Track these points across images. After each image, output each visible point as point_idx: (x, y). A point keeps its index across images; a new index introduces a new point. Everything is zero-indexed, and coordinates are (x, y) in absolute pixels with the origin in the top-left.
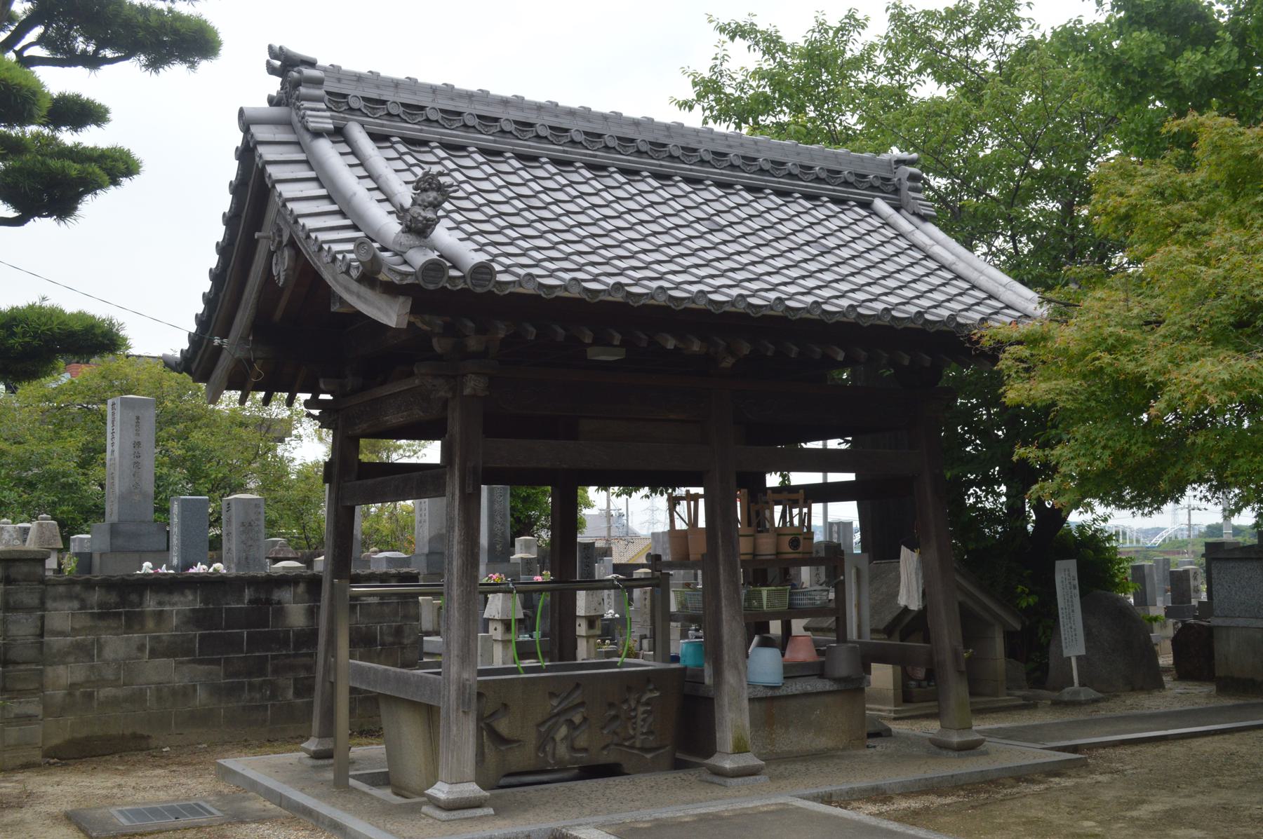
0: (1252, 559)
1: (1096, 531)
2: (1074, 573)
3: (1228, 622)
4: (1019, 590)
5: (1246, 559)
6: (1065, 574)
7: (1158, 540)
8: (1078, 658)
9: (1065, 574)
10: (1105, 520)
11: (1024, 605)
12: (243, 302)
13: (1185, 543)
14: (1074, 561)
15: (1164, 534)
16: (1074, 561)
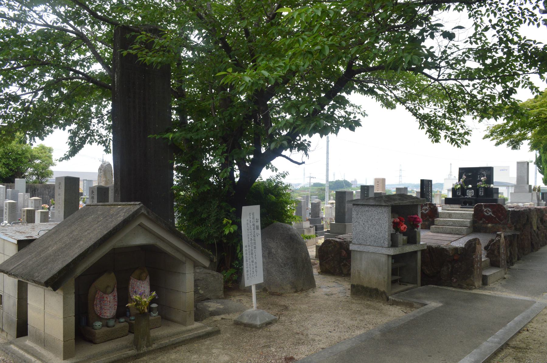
0: (381, 206)
1: (278, 183)
2: (258, 216)
3: (361, 248)
4: (225, 222)
5: (378, 205)
6: (251, 215)
7: (299, 187)
8: (258, 286)
9: (251, 215)
10: (284, 176)
11: (227, 232)
12: (440, 234)
13: (308, 188)
14: (258, 207)
15: (301, 186)
16: (258, 207)
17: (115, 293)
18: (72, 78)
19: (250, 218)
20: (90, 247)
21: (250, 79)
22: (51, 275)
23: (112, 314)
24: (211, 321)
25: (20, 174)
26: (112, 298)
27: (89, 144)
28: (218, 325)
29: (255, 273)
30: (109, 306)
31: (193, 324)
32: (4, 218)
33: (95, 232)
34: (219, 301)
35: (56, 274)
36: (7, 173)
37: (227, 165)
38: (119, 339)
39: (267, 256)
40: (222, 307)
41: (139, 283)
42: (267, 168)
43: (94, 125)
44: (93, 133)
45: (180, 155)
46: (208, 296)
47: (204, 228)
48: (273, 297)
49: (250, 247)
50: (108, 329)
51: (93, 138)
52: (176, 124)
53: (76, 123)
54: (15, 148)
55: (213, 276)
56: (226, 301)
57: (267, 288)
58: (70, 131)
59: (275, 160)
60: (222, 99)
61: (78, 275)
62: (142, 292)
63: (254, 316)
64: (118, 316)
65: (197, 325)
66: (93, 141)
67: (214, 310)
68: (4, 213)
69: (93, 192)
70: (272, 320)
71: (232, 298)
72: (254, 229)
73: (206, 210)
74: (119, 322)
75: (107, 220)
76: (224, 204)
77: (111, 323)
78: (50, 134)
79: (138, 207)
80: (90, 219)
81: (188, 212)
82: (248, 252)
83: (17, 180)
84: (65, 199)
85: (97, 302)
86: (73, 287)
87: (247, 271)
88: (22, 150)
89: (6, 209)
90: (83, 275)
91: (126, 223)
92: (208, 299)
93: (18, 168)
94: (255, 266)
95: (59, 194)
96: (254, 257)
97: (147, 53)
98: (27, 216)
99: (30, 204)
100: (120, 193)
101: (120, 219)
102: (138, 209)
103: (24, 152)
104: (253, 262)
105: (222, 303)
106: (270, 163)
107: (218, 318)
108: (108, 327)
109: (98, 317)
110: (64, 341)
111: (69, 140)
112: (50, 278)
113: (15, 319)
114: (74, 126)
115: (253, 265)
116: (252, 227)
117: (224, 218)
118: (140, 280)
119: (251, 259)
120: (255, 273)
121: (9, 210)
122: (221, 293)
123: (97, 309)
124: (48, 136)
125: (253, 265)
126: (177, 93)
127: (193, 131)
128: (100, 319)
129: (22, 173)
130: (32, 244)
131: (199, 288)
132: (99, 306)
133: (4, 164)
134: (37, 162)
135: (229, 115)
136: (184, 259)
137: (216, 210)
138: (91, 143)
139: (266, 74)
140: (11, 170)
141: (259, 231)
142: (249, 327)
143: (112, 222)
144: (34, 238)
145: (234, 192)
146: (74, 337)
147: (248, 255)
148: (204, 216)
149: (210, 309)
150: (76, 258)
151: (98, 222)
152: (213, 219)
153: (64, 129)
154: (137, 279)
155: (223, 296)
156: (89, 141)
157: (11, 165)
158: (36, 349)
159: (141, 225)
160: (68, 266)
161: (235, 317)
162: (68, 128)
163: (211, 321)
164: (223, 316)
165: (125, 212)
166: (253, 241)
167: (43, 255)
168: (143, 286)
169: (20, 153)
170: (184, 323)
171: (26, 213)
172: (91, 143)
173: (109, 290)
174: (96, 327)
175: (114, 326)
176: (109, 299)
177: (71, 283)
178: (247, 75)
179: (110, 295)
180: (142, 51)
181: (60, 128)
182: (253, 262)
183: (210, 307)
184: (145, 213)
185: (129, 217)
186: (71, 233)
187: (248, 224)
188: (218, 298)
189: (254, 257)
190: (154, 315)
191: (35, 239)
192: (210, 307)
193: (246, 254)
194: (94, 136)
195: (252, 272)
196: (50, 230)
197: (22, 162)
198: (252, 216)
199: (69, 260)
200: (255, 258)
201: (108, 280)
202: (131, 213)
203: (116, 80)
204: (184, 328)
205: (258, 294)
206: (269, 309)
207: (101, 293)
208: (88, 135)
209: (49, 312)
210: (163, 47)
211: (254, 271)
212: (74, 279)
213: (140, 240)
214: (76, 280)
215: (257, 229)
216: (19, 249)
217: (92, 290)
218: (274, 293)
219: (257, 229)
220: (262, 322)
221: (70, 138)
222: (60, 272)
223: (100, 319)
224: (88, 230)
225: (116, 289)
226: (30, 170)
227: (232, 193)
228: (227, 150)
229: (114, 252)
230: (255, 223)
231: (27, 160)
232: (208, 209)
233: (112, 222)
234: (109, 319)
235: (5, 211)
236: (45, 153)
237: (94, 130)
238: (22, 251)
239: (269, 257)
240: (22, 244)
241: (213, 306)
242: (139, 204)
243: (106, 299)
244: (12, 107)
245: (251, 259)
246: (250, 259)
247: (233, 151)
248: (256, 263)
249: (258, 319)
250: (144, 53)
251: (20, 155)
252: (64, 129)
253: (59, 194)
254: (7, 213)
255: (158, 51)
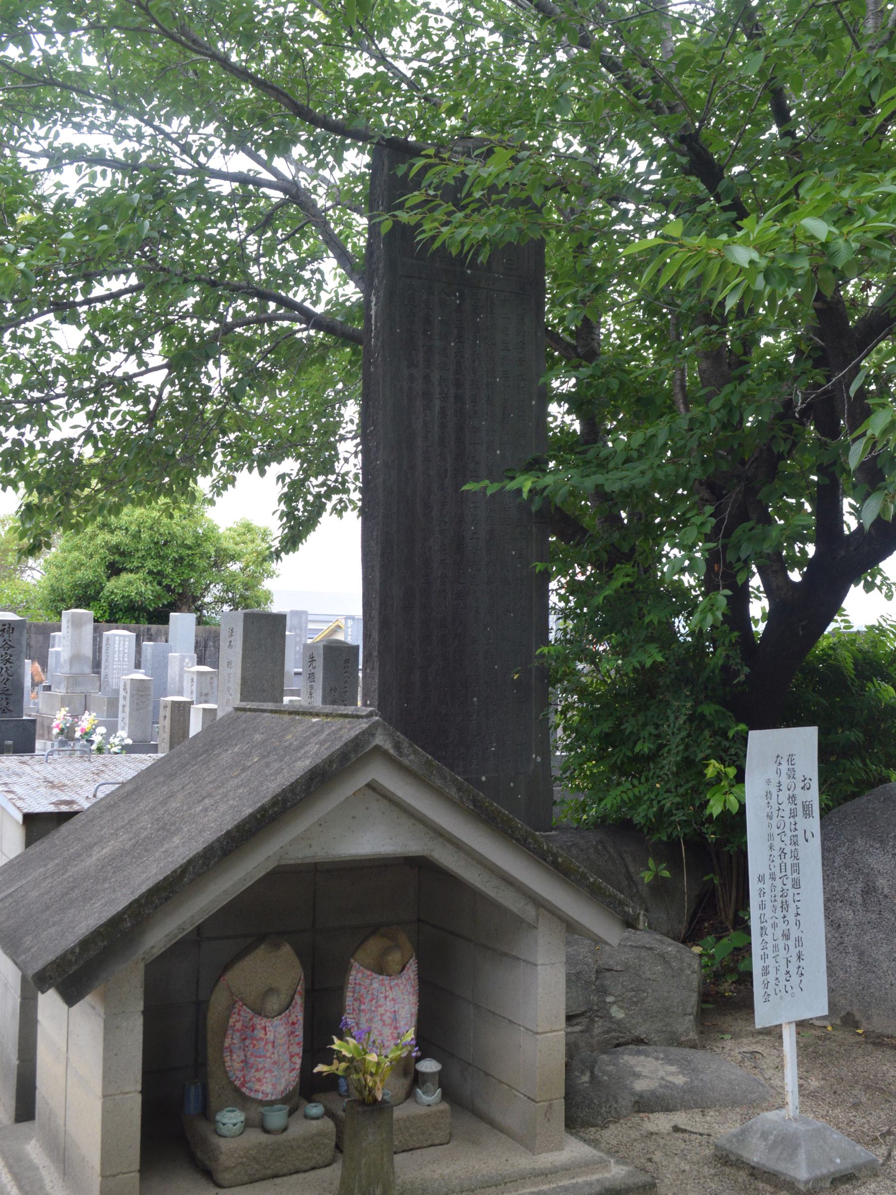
2: (808, 764)
4: (710, 772)
17: (298, 1013)
18: (271, 320)
19: (779, 772)
20: (190, 862)
21: (755, 256)
22: (59, 951)
23: (281, 1088)
24: (634, 1134)
25: (185, 599)
26: (282, 1030)
27: (334, 516)
28: (658, 1156)
29: (795, 979)
30: (268, 1056)
31: (560, 1147)
32: (120, 724)
33: (223, 808)
34: (676, 1052)
35: (72, 951)
36: (158, 597)
37: (723, 575)
38: (300, 1176)
39: (859, 900)
40: (680, 1080)
41: (377, 983)
42: (869, 587)
43: (346, 460)
44: (344, 482)
45: (577, 545)
46: (641, 1031)
47: (643, 788)
48: (879, 1054)
49: (778, 883)
50: (264, 1138)
51: (345, 497)
52: (567, 444)
53: (298, 456)
54: (177, 530)
55: (663, 958)
56: (698, 1056)
57: (858, 1016)
58: (281, 477)
59: (889, 559)
60: (706, 356)
61: (157, 952)
62: (384, 1013)
63: (786, 1143)
64: (310, 1087)
65: (575, 1150)
66: (345, 508)
67: (653, 1092)
68: (120, 708)
69: (312, 659)
70: (859, 1168)
71: (729, 1044)
72: (793, 814)
73: (651, 729)
74: (306, 1117)
75: (267, 765)
76: (708, 709)
77: (276, 1118)
78: (230, 486)
79: (364, 725)
80: (226, 757)
81: (596, 731)
82: (767, 898)
83: (172, 615)
84: (244, 679)
85: (232, 1040)
86: (139, 992)
87: (765, 971)
88: (197, 537)
89: (125, 698)
90: (181, 948)
91: (319, 780)
92: (639, 1041)
93: (184, 583)
94: (794, 952)
95: (229, 663)
96: (791, 916)
97: (450, 214)
98: (172, 720)
99: (186, 684)
100: (377, 665)
101: (303, 765)
102: (363, 733)
103: (199, 541)
104: (786, 936)
105: (686, 1066)
106: (880, 572)
107: (661, 1122)
108: (266, 1131)
109: (237, 1090)
110: (104, 1176)
111: (283, 507)
112: (223, 908)
113: (15, 1062)
114: (291, 466)
115: (787, 948)
116: (787, 807)
117: (707, 758)
118: (381, 973)
119: (782, 926)
120: (795, 979)
121: (132, 702)
122: (686, 1026)
123: (234, 1063)
124: (224, 493)
125: (787, 948)
126: (574, 348)
127: (611, 465)
128: (241, 1099)
129: (195, 599)
130: (65, 828)
131: (610, 999)
132: (238, 1056)
133: (150, 572)
134: (234, 567)
135: (724, 406)
136: (530, 912)
137: (684, 733)
138: (340, 513)
139: (820, 228)
140: (168, 588)
141: (814, 824)
142: (768, 1182)
143: (279, 771)
144: (75, 808)
145: (747, 670)
146: (136, 1166)
147: (768, 912)
148: (644, 747)
149: (640, 1086)
150: (141, 897)
151: (244, 770)
152: (670, 762)
153: (262, 473)
154: (372, 970)
155: (693, 1035)
156: (334, 508)
157: (167, 576)
158: (41, 1180)
159: (372, 786)
160: (115, 922)
161: (723, 1127)
162: (274, 469)
163: (634, 1134)
164: (680, 1118)
165: (322, 743)
166: (789, 861)
167: (72, 871)
168: (391, 995)
169: (188, 542)
170: (526, 1141)
171: (169, 709)
172: (340, 513)
173: (273, 1003)
174: (224, 1130)
175: (285, 1129)
176: (270, 1036)
177: (129, 978)
178: (745, 242)
179: (276, 1021)
180: (432, 210)
181: (250, 469)
182: (786, 936)
183: (637, 1076)
184: (388, 746)
185: (329, 761)
186: (164, 803)
187: (768, 794)
188: (674, 1041)
189: (791, 916)
190: (426, 1099)
191: (76, 813)
192: (637, 1076)
193: (762, 906)
194: (347, 491)
195: (782, 977)
196: (123, 784)
197: (192, 567)
198: (784, 767)
199: (122, 900)
200: (798, 923)
201: (275, 970)
202: (338, 745)
203: (373, 313)
204: (523, 1162)
205: (803, 1049)
206: (856, 1106)
207: (246, 1013)
208: (331, 491)
209: (83, 1058)
210: (492, 189)
211: (793, 969)
212: (142, 966)
213: (373, 839)
214: (148, 967)
215: (807, 813)
216: (30, 840)
217: (219, 1000)
218: (880, 1036)
219: (807, 813)
220: (818, 1173)
221: (287, 498)
222: (85, 944)
223: (241, 1099)
224: (209, 795)
225: (299, 1000)
226: (216, 590)
227: (737, 674)
228: (716, 528)
229: (279, 876)
230: (798, 792)
231: (203, 564)
232: (657, 726)
233: (279, 771)
234: (271, 1103)
235: (121, 702)
236: (253, 541)
237: (347, 473)
238: (38, 847)
239: (864, 904)
240: (37, 825)
241: (650, 1071)
242: (370, 715)
243: (261, 1034)
244: (117, 413)
245: (782, 926)
246: (774, 926)
247: (738, 532)
248: (799, 940)
249: (802, 1156)
250: (440, 214)
251: (190, 548)
252: (262, 473)
253: (229, 663)
254: (127, 709)
255: (484, 205)
